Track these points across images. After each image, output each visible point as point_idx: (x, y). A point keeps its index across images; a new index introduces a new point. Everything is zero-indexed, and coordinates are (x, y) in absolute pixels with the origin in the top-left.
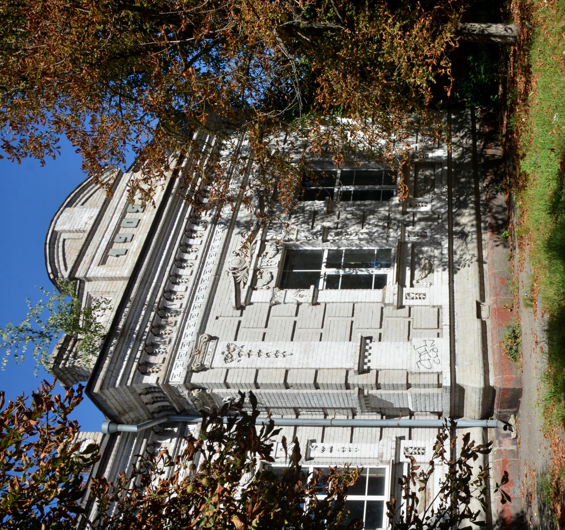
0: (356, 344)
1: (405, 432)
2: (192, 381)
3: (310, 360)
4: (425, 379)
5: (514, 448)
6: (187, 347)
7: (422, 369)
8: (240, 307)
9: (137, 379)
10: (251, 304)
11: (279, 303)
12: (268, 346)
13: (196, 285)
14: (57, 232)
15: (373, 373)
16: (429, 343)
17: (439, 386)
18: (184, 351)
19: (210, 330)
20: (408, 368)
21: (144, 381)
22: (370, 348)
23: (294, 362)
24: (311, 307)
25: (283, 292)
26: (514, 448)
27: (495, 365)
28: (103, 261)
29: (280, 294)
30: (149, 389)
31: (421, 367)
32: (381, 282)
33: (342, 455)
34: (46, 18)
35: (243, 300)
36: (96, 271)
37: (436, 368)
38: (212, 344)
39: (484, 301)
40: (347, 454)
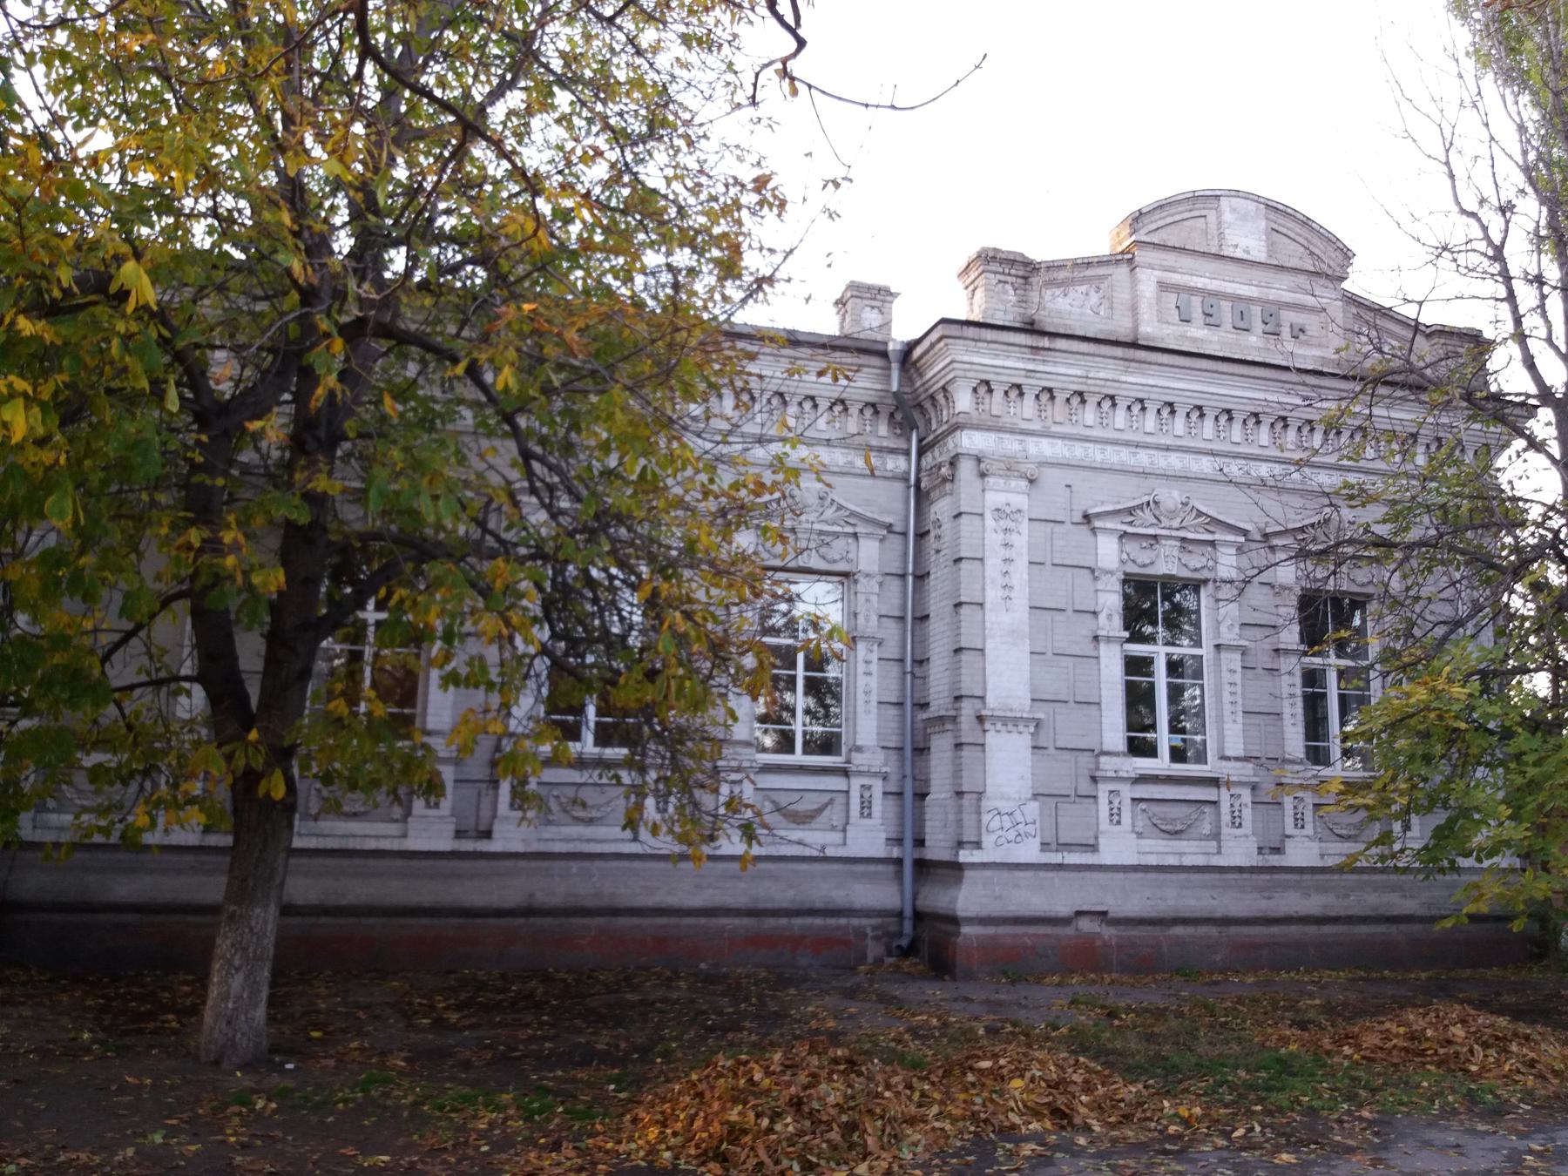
7: (986, 818)
18: (1011, 444)
27: (994, 937)
28: (1163, 287)
31: (990, 816)
33: (860, 691)
37: (988, 841)
38: (1024, 484)
40: (861, 696)
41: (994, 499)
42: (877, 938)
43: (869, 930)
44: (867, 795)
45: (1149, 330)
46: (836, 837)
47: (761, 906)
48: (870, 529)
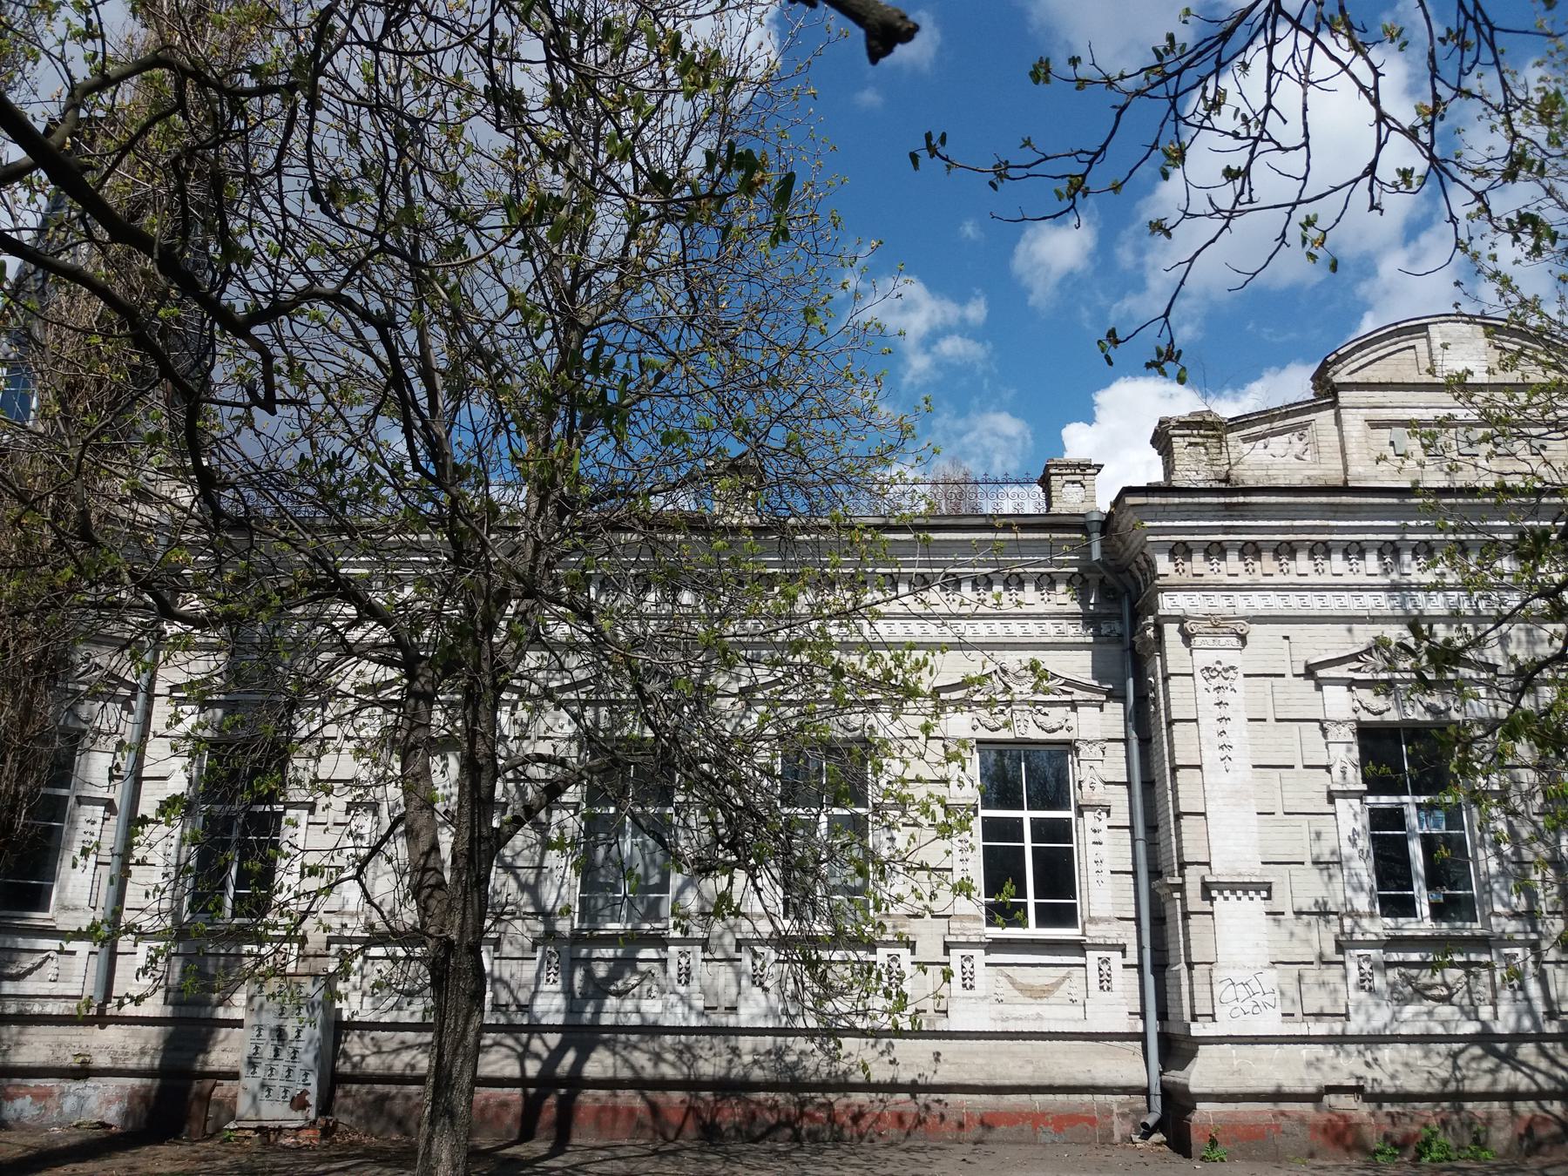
0: (1256, 873)
1: (1132, 958)
2: (1166, 626)
3: (1220, 802)
4: (1201, 993)
5: (1117, 1138)
6: (1226, 603)
7: (1217, 989)
8: (1310, 672)
9: (1159, 547)
10: (1319, 688)
11: (1325, 736)
12: (1239, 731)
13: (1347, 588)
14: (1427, 330)
15: (1206, 906)
16: (1269, 999)
17: (1194, 1018)
18: (1219, 603)
19: (1256, 632)
20: (1220, 964)
21: (1158, 557)
22: (1226, 899)
23: (1214, 776)
24: (1325, 789)
25: (1351, 738)
26: (1117, 1138)
27: (1233, 1114)
28: (1375, 425)
29: (1347, 734)
30: (1151, 565)
31: (1222, 987)
32: (1401, 906)
33: (1091, 860)
34: (773, 770)
35: (1321, 673)
36: (1354, 422)
37: (1220, 1013)
38: (1234, 641)
39: (1364, 1100)
40: (1093, 867)
41: (1203, 658)
42: (1123, 1116)
43: (1115, 1107)
44: (968, 965)
45: (1360, 469)
46: (1077, 1011)
47: (998, 1082)
48: (1088, 695)
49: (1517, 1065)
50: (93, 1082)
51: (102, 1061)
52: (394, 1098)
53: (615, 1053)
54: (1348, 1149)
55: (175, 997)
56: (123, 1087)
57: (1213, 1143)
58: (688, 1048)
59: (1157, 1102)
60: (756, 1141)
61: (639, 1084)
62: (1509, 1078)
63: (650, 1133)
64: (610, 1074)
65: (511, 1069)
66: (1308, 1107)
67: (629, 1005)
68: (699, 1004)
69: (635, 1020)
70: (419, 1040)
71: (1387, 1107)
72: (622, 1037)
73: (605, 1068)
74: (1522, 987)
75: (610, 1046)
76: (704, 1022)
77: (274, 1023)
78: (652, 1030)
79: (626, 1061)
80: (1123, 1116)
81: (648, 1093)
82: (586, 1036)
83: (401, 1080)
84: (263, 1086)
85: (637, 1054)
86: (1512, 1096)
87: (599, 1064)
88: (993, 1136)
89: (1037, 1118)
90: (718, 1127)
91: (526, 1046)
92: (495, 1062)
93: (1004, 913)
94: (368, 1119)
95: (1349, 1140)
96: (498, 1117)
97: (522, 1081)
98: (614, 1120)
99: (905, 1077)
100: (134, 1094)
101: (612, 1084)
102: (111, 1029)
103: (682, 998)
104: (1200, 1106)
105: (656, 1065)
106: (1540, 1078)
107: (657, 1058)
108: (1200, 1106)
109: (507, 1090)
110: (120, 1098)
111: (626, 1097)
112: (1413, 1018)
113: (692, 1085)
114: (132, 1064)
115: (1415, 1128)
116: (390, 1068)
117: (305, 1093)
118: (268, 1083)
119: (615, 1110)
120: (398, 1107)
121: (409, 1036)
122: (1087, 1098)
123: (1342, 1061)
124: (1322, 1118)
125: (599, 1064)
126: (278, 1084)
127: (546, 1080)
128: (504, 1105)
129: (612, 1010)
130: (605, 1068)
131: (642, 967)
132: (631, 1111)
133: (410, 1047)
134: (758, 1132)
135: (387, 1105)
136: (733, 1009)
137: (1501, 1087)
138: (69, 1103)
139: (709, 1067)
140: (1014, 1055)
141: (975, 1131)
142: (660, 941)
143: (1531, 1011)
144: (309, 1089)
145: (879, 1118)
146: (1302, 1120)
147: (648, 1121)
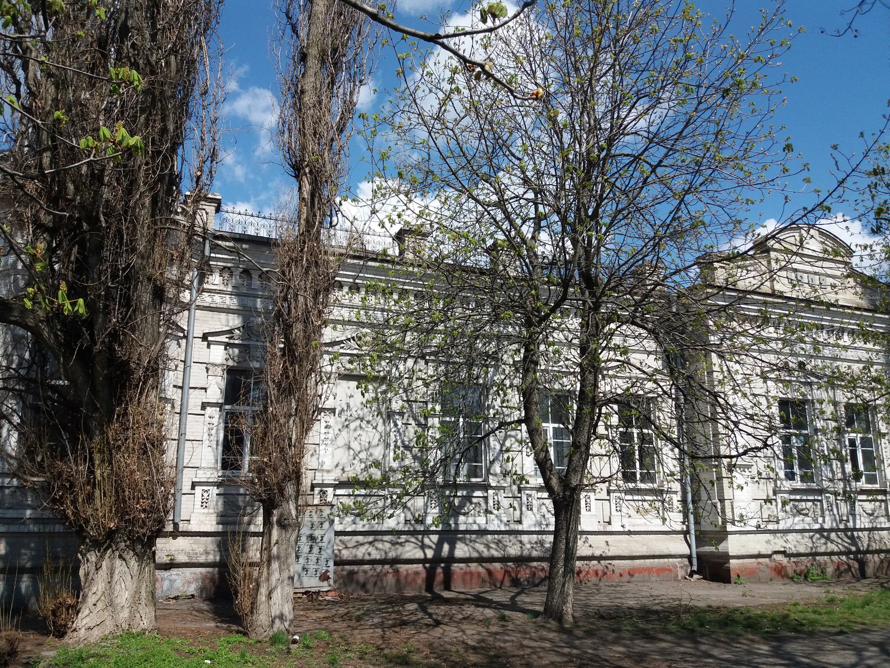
5: (680, 578)
11: (207, 372)
26: (680, 578)
27: (743, 564)
42: (682, 567)
44: (206, 495)
47: (634, 554)
49: (832, 541)
50: (174, 571)
51: (182, 558)
52: (357, 573)
53: (467, 545)
54: (783, 577)
55: (223, 518)
56: (195, 574)
57: (739, 576)
58: (500, 541)
59: (695, 561)
60: (537, 586)
61: (481, 560)
62: (832, 547)
63: (488, 585)
64: (468, 555)
65: (419, 554)
66: (767, 560)
67: (470, 520)
68: (505, 519)
69: (475, 527)
70: (366, 540)
71: (792, 559)
72: (468, 536)
73: (465, 552)
74: (832, 510)
75: (463, 540)
76: (507, 528)
77: (309, 532)
78: (483, 532)
79: (474, 548)
80: (682, 567)
81: (484, 564)
82: (450, 536)
83: (362, 562)
84: (304, 568)
85: (477, 545)
86: (832, 553)
87: (461, 551)
88: (634, 579)
89: (649, 570)
90: (519, 580)
91: (422, 542)
92: (410, 551)
93: (628, 477)
94: (345, 584)
95: (783, 573)
96: (414, 580)
97: (424, 561)
98: (471, 579)
99: (597, 553)
100: (204, 578)
101: (467, 560)
102: (180, 540)
103: (497, 516)
104: (731, 561)
105: (488, 550)
106: (840, 546)
107: (488, 547)
108: (731, 561)
109: (415, 565)
110: (196, 580)
111: (474, 566)
112: (799, 522)
113: (504, 560)
114: (202, 559)
115: (803, 568)
116: (356, 556)
117: (327, 571)
118: (306, 566)
119: (471, 573)
120: (361, 578)
121: (360, 538)
122: (666, 560)
123: (776, 541)
124: (773, 564)
125: (461, 551)
126: (312, 567)
127: (437, 560)
128: (417, 573)
129: (463, 522)
130: (465, 552)
131: (475, 500)
132: (479, 574)
133: (362, 544)
134: (537, 582)
135: (355, 576)
136: (520, 522)
137: (829, 551)
138: (166, 584)
139: (513, 550)
140: (637, 542)
141: (626, 577)
142: (486, 487)
143: (835, 520)
144: (329, 569)
145: (588, 573)
146: (767, 565)
147: (487, 578)
